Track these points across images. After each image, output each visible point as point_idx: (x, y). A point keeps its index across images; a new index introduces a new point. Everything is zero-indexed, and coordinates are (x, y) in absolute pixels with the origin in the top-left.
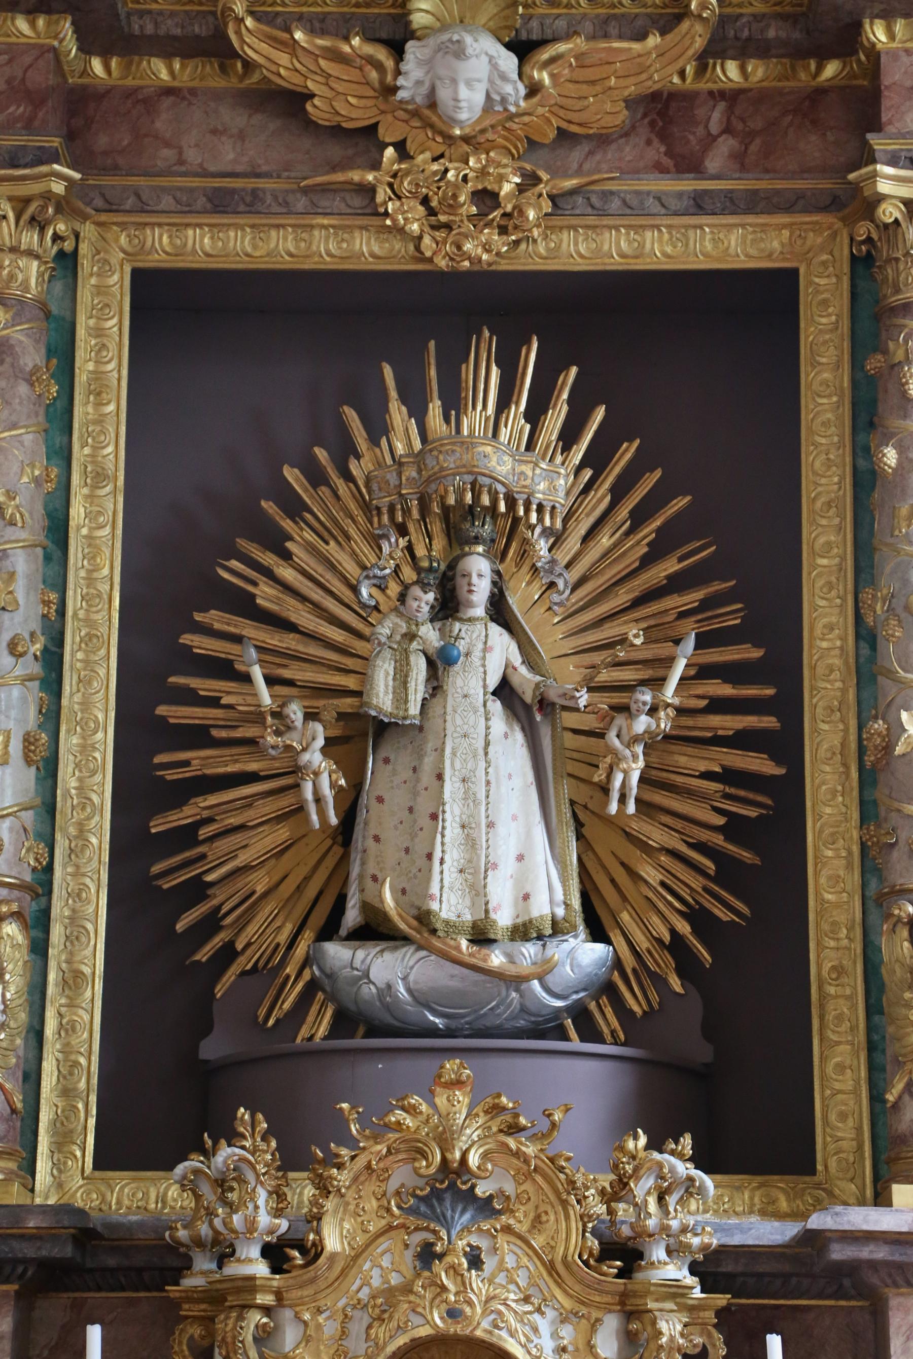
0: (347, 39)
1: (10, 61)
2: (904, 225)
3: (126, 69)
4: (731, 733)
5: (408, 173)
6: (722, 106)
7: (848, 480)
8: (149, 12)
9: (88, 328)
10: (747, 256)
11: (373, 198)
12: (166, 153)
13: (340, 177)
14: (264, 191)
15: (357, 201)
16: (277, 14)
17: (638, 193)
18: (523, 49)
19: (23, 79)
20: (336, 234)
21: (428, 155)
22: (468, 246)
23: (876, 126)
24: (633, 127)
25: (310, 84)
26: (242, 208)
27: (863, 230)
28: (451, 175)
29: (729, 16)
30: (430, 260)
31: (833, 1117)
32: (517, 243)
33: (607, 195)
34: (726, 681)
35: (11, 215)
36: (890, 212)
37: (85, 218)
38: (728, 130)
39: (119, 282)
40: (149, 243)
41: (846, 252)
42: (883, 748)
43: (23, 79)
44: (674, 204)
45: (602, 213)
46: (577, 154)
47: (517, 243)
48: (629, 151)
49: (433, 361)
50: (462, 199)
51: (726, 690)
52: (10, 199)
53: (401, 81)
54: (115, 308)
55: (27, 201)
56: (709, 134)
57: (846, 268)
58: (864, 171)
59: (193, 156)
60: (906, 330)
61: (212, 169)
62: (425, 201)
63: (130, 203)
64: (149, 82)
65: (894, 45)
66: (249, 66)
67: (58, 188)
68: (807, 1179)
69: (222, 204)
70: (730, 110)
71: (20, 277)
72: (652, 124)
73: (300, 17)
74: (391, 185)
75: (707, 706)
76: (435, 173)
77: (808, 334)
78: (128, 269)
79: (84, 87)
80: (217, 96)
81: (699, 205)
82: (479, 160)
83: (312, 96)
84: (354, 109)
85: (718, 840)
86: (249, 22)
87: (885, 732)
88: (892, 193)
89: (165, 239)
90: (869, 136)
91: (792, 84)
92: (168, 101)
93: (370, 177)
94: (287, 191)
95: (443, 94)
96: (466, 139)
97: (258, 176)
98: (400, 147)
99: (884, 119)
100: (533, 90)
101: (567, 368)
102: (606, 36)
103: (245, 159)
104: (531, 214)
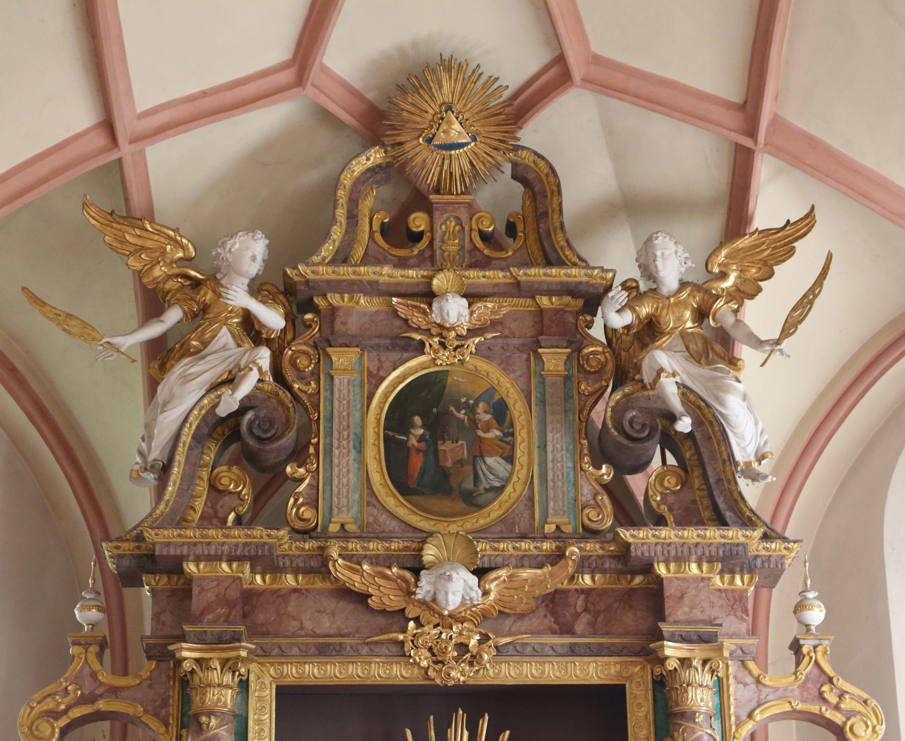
0: (389, 567)
1: (218, 585)
3: (273, 581)
5: (422, 634)
6: (582, 597)
8: (288, 555)
9: (254, 720)
10: (598, 677)
11: (403, 647)
12: (294, 623)
13: (385, 637)
14: (345, 644)
15: (394, 649)
16: (353, 555)
17: (540, 644)
18: (480, 573)
19: (224, 595)
20: (383, 666)
21: (432, 626)
22: (453, 674)
23: (663, 619)
24: (537, 608)
25: (370, 590)
26: (334, 653)
27: (658, 670)
28: (443, 636)
29: (585, 556)
30: (434, 680)
32: (478, 671)
33: (524, 645)
35: (219, 668)
36: (672, 664)
37: (252, 661)
38: (586, 610)
39: (270, 694)
40: (285, 671)
41: (650, 677)
43: (224, 595)
44: (560, 650)
45: (523, 655)
46: (508, 623)
47: (478, 671)
48: (534, 621)
49: (432, 727)
50: (450, 649)
52: (218, 659)
53: (418, 591)
54: (268, 708)
55: (227, 660)
56: (577, 612)
57: (650, 686)
58: (657, 644)
59: (308, 625)
61: (318, 631)
62: (430, 649)
63: (277, 650)
64: (284, 586)
65: (670, 575)
66: (337, 580)
67: (244, 654)
69: (324, 651)
70: (586, 601)
71: (223, 699)
72: (547, 606)
73: (365, 556)
74: (412, 641)
76: (435, 634)
78: (274, 686)
79: (251, 590)
80: (320, 592)
81: (573, 651)
82: (458, 627)
83: (371, 596)
84: (393, 601)
86: (340, 561)
89: (294, 670)
90: (660, 624)
91: (619, 586)
92: (294, 596)
93: (401, 637)
94: (358, 644)
95: (440, 597)
96: (450, 616)
97: (343, 636)
98: (417, 620)
99: (666, 613)
100: (486, 593)
101: (504, 731)
102: (523, 566)
103: (335, 626)
104: (486, 657)
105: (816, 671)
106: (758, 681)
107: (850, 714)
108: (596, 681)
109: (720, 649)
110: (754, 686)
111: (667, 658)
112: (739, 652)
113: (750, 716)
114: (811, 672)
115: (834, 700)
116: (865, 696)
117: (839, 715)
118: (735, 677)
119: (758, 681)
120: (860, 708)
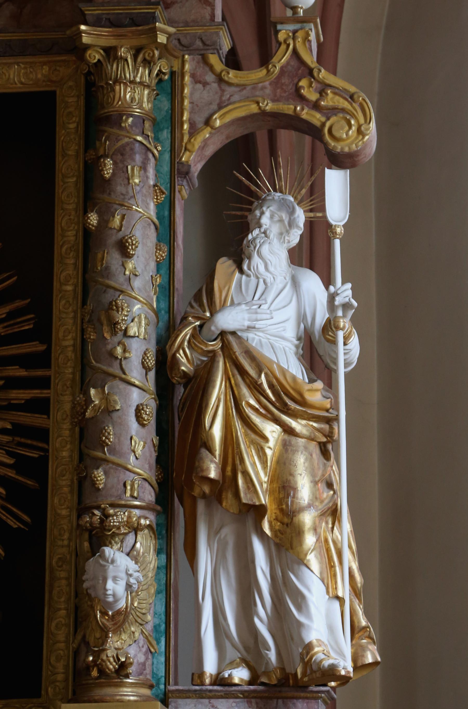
2: (104, 63)
4: (23, 402)
7: (81, 233)
31: (53, 659)
34: (22, 367)
36: (94, 56)
42: (82, 414)
51: (23, 373)
60: (106, 134)
68: (35, 700)
75: (4, 384)
77: (61, 135)
85: (11, 474)
87: (83, 403)
88: (93, 43)
105: (294, 63)
106: (220, 80)
107: (334, 110)
108: (18, 88)
109: (153, 32)
110: (215, 85)
111: (87, 47)
112: (198, 43)
113: (208, 122)
114: (288, 63)
115: (313, 96)
116: (352, 89)
117: (318, 115)
118: (193, 76)
119: (220, 80)
120: (345, 104)
